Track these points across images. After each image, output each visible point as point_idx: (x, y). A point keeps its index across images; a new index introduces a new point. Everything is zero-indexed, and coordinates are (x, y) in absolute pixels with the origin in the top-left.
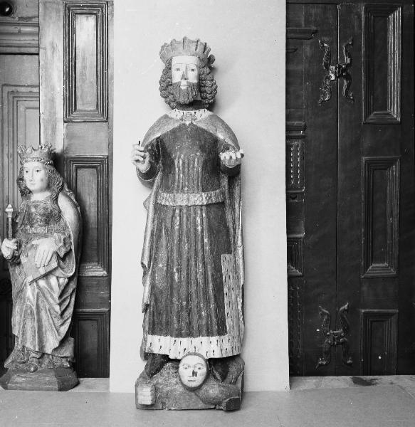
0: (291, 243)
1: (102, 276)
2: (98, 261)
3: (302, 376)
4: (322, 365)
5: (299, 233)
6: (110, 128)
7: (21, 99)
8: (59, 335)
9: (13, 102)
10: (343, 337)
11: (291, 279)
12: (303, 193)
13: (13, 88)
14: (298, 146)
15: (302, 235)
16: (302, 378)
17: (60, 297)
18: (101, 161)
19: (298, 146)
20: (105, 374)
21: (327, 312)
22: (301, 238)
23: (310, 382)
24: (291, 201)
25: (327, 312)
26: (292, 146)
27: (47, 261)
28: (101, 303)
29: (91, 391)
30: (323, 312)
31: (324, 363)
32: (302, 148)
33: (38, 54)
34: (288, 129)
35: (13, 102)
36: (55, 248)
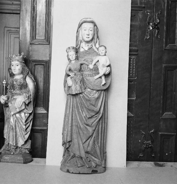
0: (129, 101)
1: (45, 113)
2: (43, 107)
3: (132, 161)
4: (141, 156)
5: (133, 97)
6: (51, 48)
7: (12, 33)
8: (24, 139)
9: (9, 35)
10: (150, 144)
11: (128, 117)
12: (136, 80)
13: (9, 29)
14: (134, 59)
15: (134, 98)
16: (132, 162)
17: (26, 122)
18: (46, 62)
19: (134, 59)
20: (44, 156)
21: (144, 133)
22: (133, 100)
23: (135, 164)
24: (130, 83)
25: (144, 133)
26: (131, 58)
27: (20, 106)
28: (44, 125)
29: (37, 164)
30: (142, 133)
31: (142, 156)
32: (136, 60)
33: (19, 14)
34: (130, 51)
35: (9, 35)
36: (23, 100)
